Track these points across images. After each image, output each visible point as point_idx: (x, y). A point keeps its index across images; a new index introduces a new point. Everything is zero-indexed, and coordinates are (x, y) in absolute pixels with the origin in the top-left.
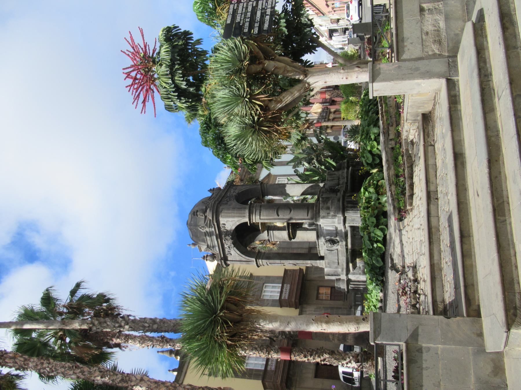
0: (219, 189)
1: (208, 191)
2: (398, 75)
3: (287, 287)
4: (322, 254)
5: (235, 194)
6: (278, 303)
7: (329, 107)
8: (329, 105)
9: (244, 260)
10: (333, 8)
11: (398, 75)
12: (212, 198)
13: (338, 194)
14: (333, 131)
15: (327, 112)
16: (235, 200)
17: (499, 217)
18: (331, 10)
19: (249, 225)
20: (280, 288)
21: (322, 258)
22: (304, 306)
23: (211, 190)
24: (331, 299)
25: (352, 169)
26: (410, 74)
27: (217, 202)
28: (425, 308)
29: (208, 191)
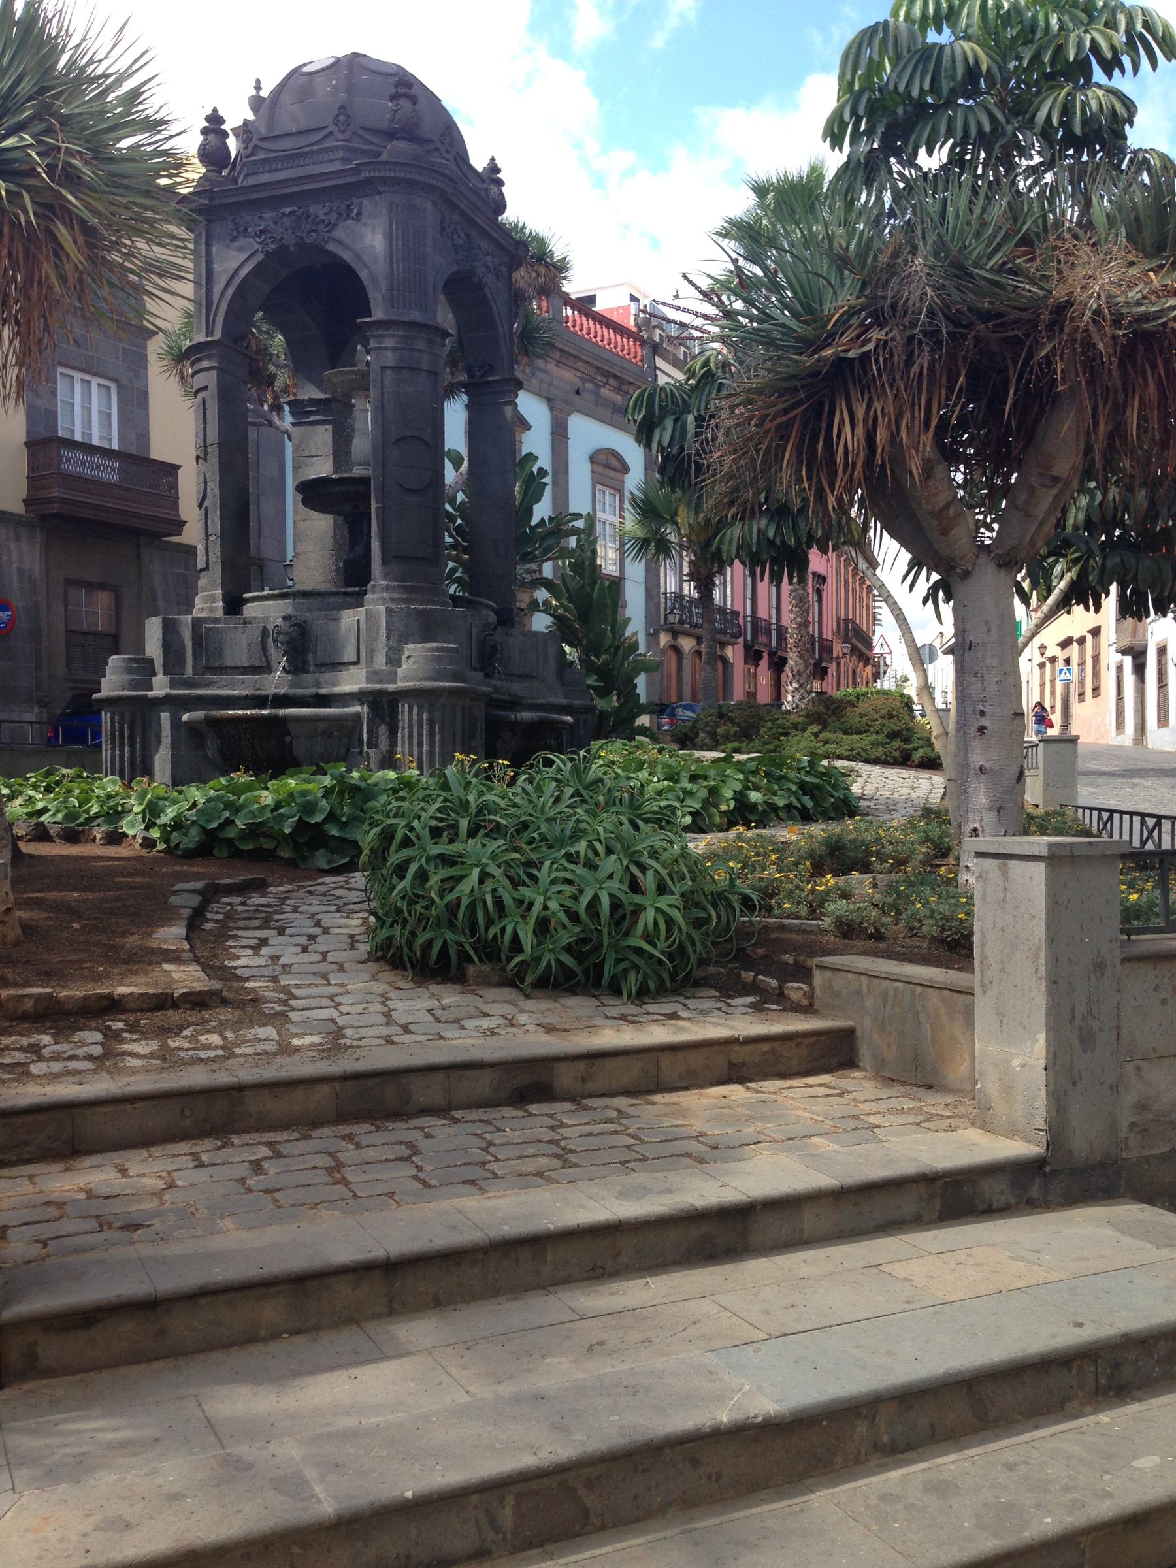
0: (501, 206)
1: (493, 159)
2: (1070, 961)
3: (110, 472)
4: (250, 610)
5: (480, 271)
6: (42, 432)
7: (741, 640)
8: (745, 640)
9: (217, 290)
10: (1053, 660)
11: (1070, 961)
12: (464, 168)
13: (481, 675)
14: (663, 652)
15: (725, 633)
16: (455, 269)
17: (510, 1501)
18: (1048, 654)
19: (358, 321)
20: (105, 445)
21: (234, 605)
22: (38, 534)
23: (498, 171)
24: (68, 632)
25: (565, 723)
26: (1073, 1010)
27: (450, 190)
28: (41, 1058)
29: (493, 159)
